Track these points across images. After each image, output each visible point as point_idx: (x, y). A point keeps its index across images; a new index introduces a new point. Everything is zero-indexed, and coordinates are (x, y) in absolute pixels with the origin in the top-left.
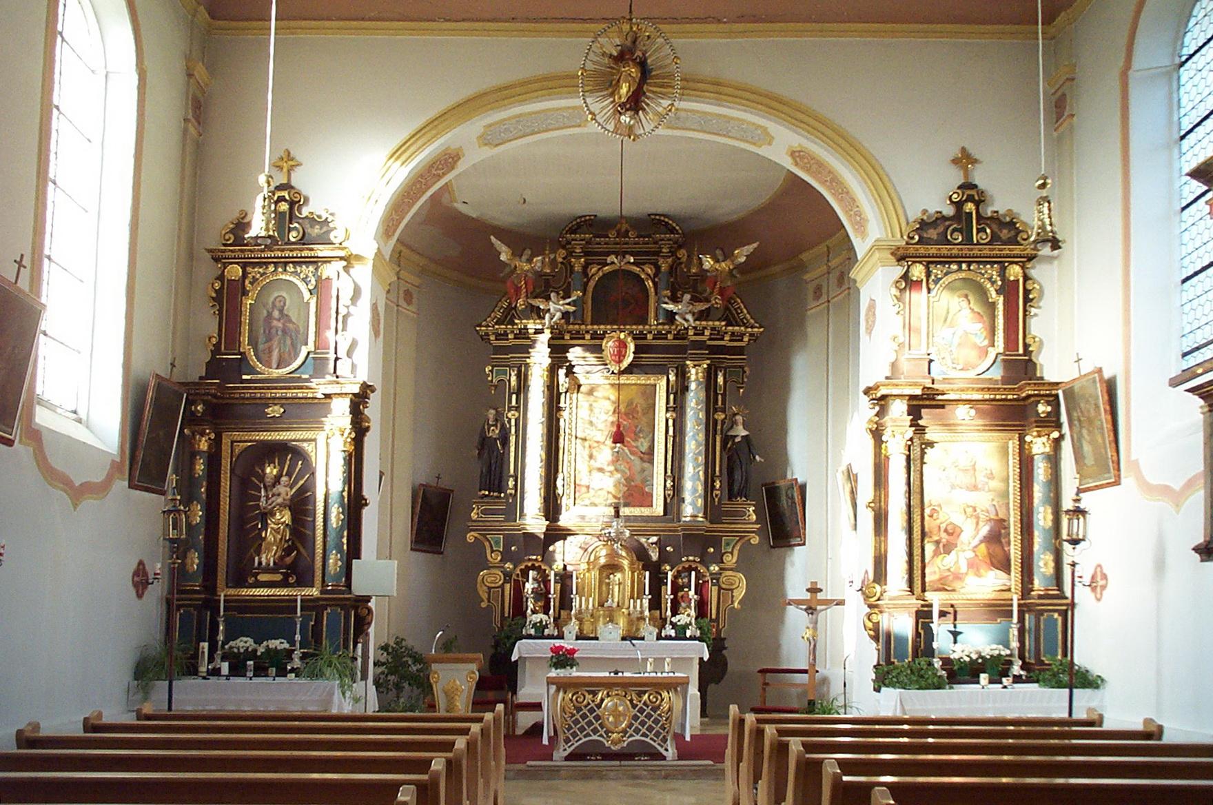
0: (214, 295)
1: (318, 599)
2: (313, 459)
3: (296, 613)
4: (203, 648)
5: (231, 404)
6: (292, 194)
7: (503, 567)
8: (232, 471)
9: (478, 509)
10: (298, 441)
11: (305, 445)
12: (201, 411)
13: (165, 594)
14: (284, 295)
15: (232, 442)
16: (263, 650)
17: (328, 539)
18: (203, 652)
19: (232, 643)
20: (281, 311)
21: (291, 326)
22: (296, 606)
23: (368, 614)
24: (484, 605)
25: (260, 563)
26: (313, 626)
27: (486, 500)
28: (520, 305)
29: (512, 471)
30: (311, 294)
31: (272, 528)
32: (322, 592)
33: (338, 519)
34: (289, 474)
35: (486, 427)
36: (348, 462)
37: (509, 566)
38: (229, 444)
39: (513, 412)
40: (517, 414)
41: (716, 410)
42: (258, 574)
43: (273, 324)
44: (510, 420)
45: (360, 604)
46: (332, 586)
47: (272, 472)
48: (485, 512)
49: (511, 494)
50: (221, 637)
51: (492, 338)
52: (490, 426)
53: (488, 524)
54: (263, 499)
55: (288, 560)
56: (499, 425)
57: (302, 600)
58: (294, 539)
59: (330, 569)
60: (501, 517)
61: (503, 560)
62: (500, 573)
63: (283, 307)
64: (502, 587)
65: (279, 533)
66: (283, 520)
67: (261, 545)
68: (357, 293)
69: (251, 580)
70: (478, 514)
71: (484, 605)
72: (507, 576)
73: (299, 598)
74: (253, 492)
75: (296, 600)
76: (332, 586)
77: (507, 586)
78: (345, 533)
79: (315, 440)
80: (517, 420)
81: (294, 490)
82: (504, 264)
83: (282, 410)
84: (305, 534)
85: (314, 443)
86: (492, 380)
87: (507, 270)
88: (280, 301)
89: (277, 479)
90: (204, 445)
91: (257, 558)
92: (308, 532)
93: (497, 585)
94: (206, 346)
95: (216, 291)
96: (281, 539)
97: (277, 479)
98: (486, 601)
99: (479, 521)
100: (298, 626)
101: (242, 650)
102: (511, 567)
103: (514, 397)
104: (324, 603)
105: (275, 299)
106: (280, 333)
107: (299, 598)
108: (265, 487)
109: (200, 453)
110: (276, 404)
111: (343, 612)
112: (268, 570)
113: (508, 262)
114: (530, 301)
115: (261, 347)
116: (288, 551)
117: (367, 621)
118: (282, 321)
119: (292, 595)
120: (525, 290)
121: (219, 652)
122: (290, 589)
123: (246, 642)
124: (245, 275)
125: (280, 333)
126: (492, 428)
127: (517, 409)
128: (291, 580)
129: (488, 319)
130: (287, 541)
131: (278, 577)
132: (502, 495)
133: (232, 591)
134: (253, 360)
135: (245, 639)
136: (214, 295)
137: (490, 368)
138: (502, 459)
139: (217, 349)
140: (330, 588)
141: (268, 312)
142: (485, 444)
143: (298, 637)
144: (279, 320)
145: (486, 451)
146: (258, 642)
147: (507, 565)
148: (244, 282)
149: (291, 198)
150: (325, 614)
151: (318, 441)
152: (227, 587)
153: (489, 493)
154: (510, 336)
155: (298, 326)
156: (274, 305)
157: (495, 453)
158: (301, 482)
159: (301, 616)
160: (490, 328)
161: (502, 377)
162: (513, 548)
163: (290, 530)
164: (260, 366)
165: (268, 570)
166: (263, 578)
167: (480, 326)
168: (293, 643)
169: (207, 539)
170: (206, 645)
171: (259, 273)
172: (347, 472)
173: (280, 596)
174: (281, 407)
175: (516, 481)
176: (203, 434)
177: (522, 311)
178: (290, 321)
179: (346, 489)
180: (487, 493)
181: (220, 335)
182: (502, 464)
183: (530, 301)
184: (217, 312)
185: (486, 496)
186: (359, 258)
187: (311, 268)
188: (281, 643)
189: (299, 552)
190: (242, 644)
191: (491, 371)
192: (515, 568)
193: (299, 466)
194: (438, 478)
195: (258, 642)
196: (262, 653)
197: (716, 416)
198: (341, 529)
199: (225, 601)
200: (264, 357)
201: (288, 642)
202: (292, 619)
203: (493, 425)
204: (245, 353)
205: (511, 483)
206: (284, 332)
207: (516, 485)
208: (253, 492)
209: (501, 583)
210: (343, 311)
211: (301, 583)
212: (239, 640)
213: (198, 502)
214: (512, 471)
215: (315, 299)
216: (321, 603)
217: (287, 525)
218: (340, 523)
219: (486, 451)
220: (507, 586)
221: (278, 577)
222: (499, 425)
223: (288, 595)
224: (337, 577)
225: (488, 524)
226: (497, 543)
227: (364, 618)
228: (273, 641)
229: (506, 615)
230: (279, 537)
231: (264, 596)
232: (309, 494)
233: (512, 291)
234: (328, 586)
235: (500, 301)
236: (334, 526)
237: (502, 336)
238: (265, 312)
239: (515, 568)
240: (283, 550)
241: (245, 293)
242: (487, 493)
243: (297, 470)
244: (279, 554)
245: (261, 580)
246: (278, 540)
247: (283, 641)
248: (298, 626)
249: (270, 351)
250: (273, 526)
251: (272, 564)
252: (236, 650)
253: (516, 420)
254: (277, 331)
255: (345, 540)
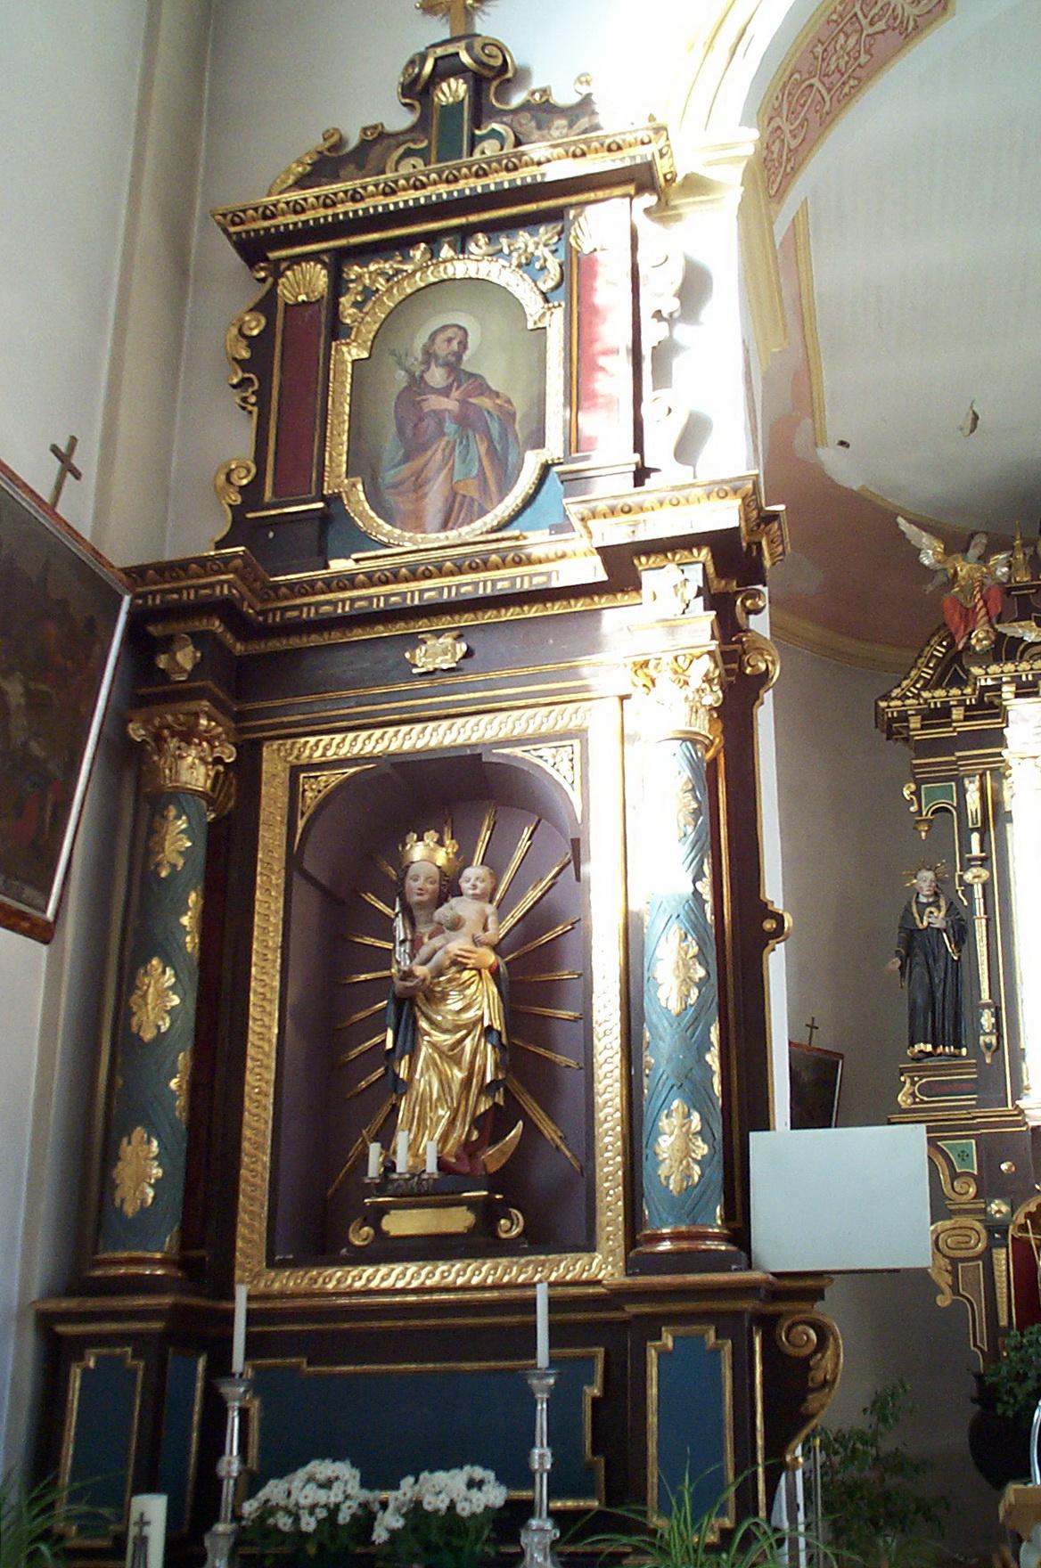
0: (245, 354)
1: (618, 1296)
2: (575, 797)
3: (533, 1355)
4: (143, 1522)
5: (300, 652)
6: (478, 49)
7: (984, 1211)
8: (293, 862)
9: (913, 1083)
10: (519, 742)
11: (546, 751)
12: (189, 667)
13: (35, 1292)
14: (463, 320)
15: (295, 771)
16: (398, 1523)
17: (649, 1059)
18: (142, 1541)
19: (274, 1490)
20: (453, 366)
21: (484, 402)
22: (533, 1328)
23: (821, 1345)
24: (943, 1301)
25: (390, 1167)
26: (595, 1400)
27: (928, 1062)
28: (979, 640)
29: (985, 996)
30: (547, 300)
31: (433, 1045)
32: (631, 1266)
33: (687, 981)
34: (495, 865)
35: (914, 909)
36: (706, 776)
37: (998, 1207)
38: (285, 776)
39: (974, 870)
40: (985, 874)
41: (967, 864)
42: (383, 1210)
43: (426, 408)
44: (968, 888)
45: (782, 1307)
46: (674, 1237)
47: (431, 860)
48: (927, 1090)
49: (988, 1046)
50: (230, 1464)
51: (915, 723)
52: (922, 907)
53: (941, 1115)
54: (401, 953)
55: (494, 1157)
56: (942, 903)
57: (554, 1304)
58: (515, 1086)
59: (663, 1171)
60: (969, 1100)
61: (984, 1193)
62: (978, 1226)
63: (459, 356)
64: (987, 1257)
65: (456, 1060)
66: (470, 1015)
67: (395, 1109)
68: (694, 287)
69: (360, 1236)
70: (913, 1095)
71: (943, 1301)
72: (996, 1230)
73: (542, 1295)
74: (369, 941)
75: (531, 1305)
76: (674, 1237)
77: (1000, 1256)
78: (714, 1035)
79: (580, 734)
80: (986, 886)
81: (510, 921)
82: (929, 572)
83: (462, 648)
84: (552, 1064)
85: (576, 743)
86: (919, 812)
87: (941, 578)
88: (450, 340)
89: (448, 887)
90: (193, 772)
91: (375, 1149)
92: (561, 1059)
93: (970, 1253)
94: (220, 493)
95: (252, 342)
96: (467, 1083)
97: (448, 887)
98: (948, 1291)
99: (915, 1111)
100: (542, 1407)
101: (308, 1524)
102: (1004, 1209)
103: (975, 837)
104: (646, 1309)
105: (433, 337)
106: (450, 427)
107: (542, 1295)
108: (408, 911)
109: (180, 796)
110: (438, 634)
111: (728, 1345)
112: (418, 1193)
113: (939, 567)
114: (1000, 628)
115: (389, 476)
116: (492, 1125)
117: (819, 1376)
118: (455, 394)
119: (512, 1285)
120: (983, 612)
121: (221, 1527)
122: (504, 1261)
123: (327, 1484)
124: (338, 285)
125: (450, 427)
126: (928, 910)
127: (984, 862)
128: (511, 1227)
129: (904, 683)
130: (487, 1090)
131: (458, 1220)
132: (964, 1051)
133: (287, 1281)
134: (362, 515)
135: (323, 1468)
136: (245, 354)
137: (913, 787)
138: (958, 976)
139: (252, 493)
140: (666, 1246)
141: (411, 374)
142: (914, 942)
143: (541, 1457)
144: (446, 392)
145: (920, 958)
146: (378, 1476)
147: (994, 1207)
148: (336, 304)
149: (476, 60)
150: (652, 1355)
151: (592, 737)
152: (272, 1264)
153: (935, 1047)
154: (957, 713)
155: (509, 401)
156: (429, 355)
157: (941, 963)
158: (532, 895)
159: (553, 1362)
160: (908, 698)
161: (942, 802)
162: (1004, 1167)
163: (499, 1047)
164: (388, 527)
165: (418, 1193)
166: (401, 1223)
167: (887, 697)
168: (515, 1472)
169: (197, 1085)
170: (153, 1509)
171: (382, 273)
172: (706, 810)
173: (464, 1288)
174: (459, 638)
175: (997, 1015)
176: (188, 735)
177: (985, 653)
178: (483, 388)
179: (707, 869)
180: (929, 1048)
181: (260, 458)
182: (957, 984)
183: (1000, 628)
184: (253, 399)
185: (929, 1055)
186: (695, 185)
187: (545, 232)
188: (473, 1484)
189: (531, 1130)
190: (311, 1495)
191: (917, 793)
192: (1013, 1211)
193: (523, 844)
194: (812, 1027)
195: (378, 1476)
196: (393, 1533)
197: (968, 877)
198: (693, 1022)
199: (251, 1317)
200: (403, 504)
201: (500, 1479)
202: (522, 1380)
203: (929, 904)
204: (338, 497)
205: (987, 1020)
206: (467, 420)
207: (998, 1025)
208: (369, 941)
209: (981, 1246)
210: (653, 333)
211: (540, 1240)
212: (302, 1474)
213: (167, 961)
214: (985, 996)
215: (559, 314)
216: (632, 1309)
217: (489, 1030)
218: (694, 993)
219: (920, 958)
220: (1000, 1256)
221: (458, 1220)
222: (942, 903)
223: (493, 1287)
224: (690, 1201)
225: (941, 1115)
226: (964, 1156)
227: (804, 1365)
228: (440, 1476)
229: (1003, 1322)
230: (459, 1075)
231: (403, 1291)
232: (559, 930)
233: (957, 617)
234: (662, 1238)
235: (928, 643)
236: (675, 1006)
237: (941, 714)
238: (401, 375)
239: (1013, 1211)
240: (477, 1122)
241: (337, 330)
242: (929, 1048)
243: (518, 855)
244: (460, 1133)
245: (394, 1232)
246: (456, 1088)
247: (478, 1472)
248: (542, 1407)
249: (419, 484)
250: (439, 1037)
251: (431, 1167)
252: (284, 1522)
253: (984, 886)
254: (440, 423)
255: (713, 1059)
